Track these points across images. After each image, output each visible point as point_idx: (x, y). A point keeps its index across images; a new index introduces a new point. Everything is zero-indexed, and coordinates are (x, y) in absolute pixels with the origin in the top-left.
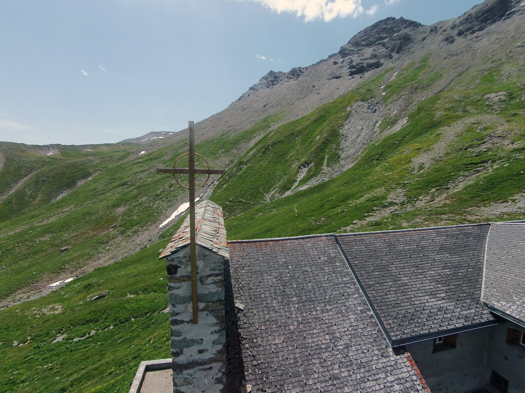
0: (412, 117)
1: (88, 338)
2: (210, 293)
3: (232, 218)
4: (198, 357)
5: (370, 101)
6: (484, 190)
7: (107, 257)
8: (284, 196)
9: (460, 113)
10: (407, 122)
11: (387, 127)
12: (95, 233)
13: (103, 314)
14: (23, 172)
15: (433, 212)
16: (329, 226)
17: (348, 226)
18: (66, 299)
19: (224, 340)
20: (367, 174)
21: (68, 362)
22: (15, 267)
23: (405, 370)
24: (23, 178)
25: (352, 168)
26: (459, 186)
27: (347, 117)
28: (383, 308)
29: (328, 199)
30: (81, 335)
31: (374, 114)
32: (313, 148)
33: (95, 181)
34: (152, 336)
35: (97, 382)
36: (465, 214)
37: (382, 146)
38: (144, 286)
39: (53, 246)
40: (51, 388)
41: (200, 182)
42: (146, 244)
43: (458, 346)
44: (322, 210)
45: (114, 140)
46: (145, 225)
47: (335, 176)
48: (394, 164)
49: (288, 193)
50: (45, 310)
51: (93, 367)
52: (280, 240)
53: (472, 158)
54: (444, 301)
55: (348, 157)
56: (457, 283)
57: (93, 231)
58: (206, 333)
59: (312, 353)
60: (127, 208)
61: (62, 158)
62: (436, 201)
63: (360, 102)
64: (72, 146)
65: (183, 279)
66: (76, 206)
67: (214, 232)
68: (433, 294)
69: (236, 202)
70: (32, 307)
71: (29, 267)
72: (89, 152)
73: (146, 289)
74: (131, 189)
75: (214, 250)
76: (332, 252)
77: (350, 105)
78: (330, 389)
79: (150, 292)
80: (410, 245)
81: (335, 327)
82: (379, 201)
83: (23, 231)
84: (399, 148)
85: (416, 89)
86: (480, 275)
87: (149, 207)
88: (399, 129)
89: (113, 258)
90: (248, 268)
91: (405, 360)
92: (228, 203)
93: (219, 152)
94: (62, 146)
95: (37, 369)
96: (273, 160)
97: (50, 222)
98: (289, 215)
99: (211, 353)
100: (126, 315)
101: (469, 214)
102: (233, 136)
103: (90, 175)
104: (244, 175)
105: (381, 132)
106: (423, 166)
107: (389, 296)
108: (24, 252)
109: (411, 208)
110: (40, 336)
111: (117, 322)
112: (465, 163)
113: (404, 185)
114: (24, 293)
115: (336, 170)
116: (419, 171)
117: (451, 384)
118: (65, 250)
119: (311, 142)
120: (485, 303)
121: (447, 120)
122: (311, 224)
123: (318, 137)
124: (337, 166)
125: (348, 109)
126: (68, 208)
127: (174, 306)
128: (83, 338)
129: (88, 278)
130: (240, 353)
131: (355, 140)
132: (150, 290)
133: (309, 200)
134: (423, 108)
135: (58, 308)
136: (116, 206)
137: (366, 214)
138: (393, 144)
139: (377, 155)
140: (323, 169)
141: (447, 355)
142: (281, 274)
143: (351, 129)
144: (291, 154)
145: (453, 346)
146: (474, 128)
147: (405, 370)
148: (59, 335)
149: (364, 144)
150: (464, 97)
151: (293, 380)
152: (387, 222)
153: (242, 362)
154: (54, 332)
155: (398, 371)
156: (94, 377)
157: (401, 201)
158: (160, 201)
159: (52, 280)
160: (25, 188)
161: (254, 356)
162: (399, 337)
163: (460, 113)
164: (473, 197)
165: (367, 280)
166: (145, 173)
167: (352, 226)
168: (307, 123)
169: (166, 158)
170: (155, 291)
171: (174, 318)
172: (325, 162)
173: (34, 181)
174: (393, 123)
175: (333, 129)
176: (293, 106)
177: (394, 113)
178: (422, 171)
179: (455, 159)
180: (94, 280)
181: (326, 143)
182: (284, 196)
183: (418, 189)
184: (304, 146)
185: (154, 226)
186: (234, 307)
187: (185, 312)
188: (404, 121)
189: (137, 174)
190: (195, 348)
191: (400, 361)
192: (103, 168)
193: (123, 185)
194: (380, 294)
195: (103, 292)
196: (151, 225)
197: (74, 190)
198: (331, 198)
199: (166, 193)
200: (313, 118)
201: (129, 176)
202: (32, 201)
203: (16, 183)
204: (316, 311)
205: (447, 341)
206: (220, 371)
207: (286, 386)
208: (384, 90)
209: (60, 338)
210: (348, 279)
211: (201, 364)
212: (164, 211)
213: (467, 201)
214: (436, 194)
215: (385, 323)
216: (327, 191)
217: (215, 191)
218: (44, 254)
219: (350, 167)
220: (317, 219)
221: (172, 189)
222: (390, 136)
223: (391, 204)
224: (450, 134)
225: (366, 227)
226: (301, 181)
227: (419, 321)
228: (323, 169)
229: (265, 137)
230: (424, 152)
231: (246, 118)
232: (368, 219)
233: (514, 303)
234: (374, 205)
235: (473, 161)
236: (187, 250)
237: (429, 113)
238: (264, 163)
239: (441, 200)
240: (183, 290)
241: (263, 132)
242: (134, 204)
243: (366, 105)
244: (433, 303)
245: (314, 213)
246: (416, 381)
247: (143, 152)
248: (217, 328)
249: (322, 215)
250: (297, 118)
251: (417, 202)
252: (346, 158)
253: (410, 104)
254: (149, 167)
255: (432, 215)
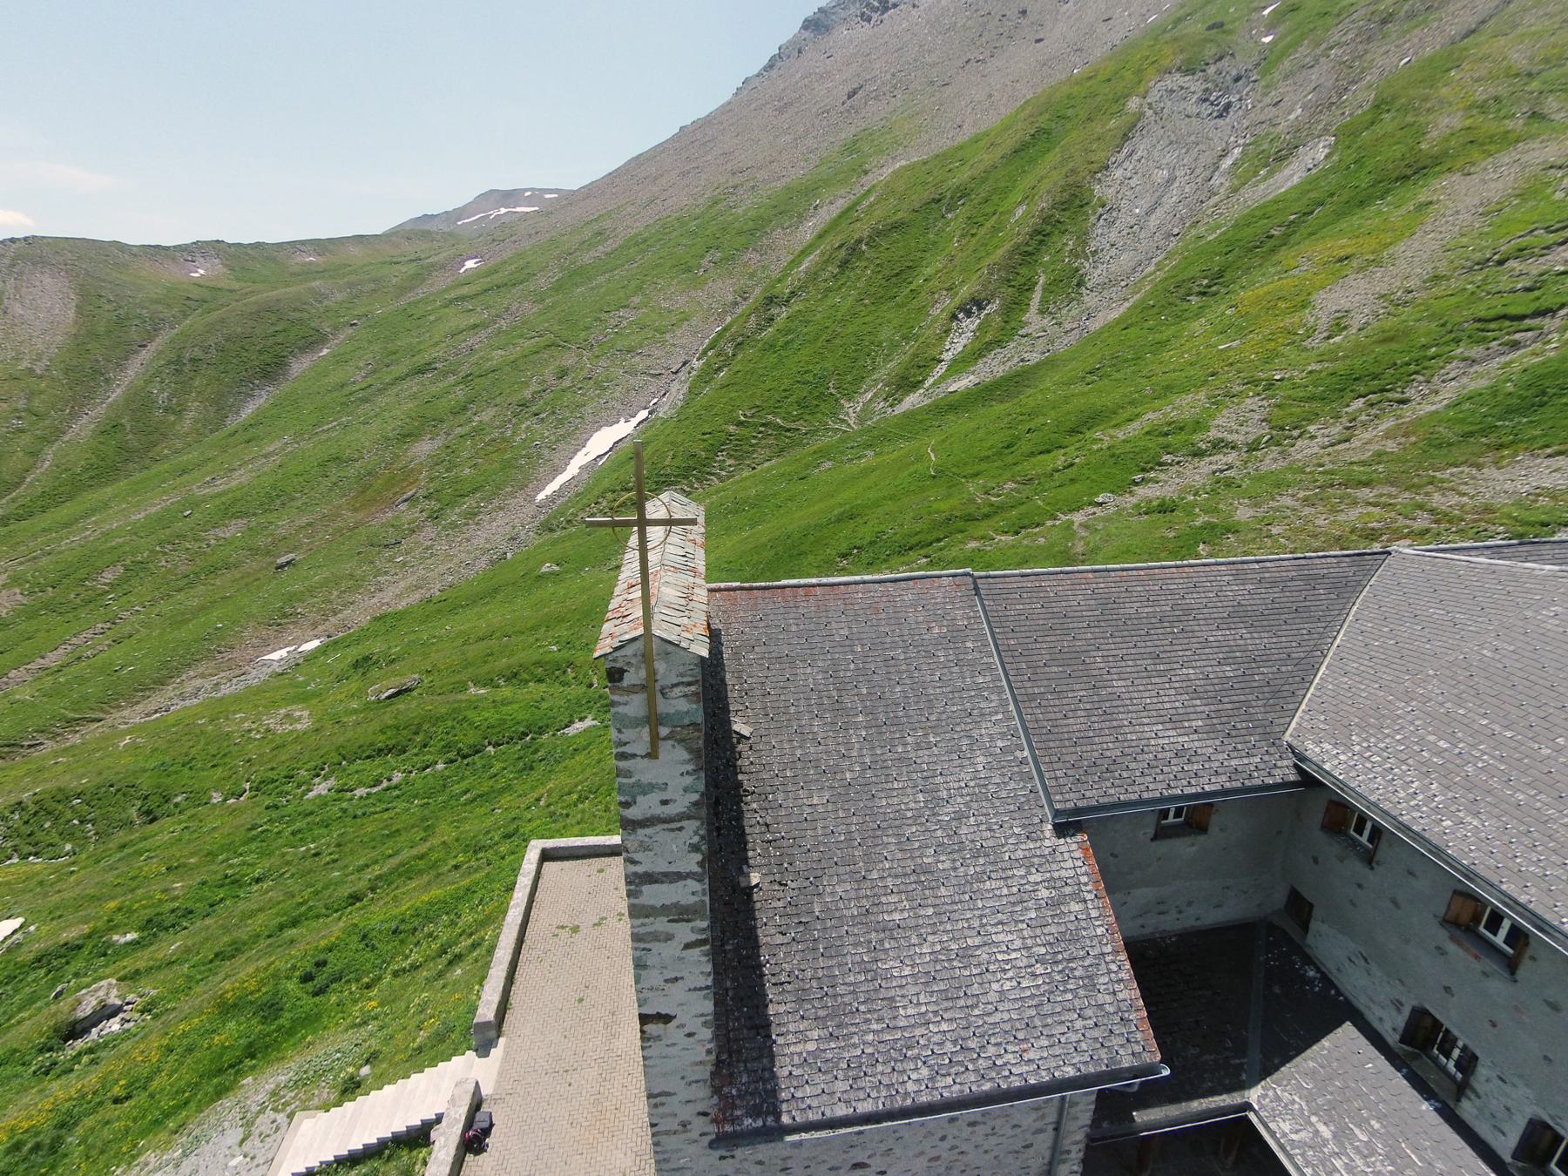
0: (1347, 135)
1: (388, 789)
2: (678, 713)
3: (745, 474)
4: (660, 811)
5: (1212, 70)
6: (1509, 412)
7: (402, 584)
8: (899, 409)
9: (1516, 124)
10: (1327, 157)
11: (1256, 173)
12: (360, 516)
13: (416, 733)
14: (134, 335)
15: (1337, 479)
16: (1023, 509)
17: (1078, 509)
18: (315, 694)
19: (702, 787)
20: (1162, 344)
21: (351, 841)
22: (165, 607)
23: (1069, 864)
24: (136, 352)
25: (1118, 321)
26: (1432, 399)
27: (1126, 137)
28: (1052, 744)
29: (1032, 425)
30: (370, 781)
31: (1220, 122)
32: (1000, 252)
33: (340, 359)
34: (541, 790)
35: (429, 884)
36: (1430, 488)
37: (1229, 244)
38: (509, 667)
39: (254, 551)
40: (327, 893)
41: (649, 362)
42: (503, 548)
43: (1214, 829)
44: (1010, 459)
45: (377, 223)
46: (495, 494)
47: (1060, 347)
48: (1254, 311)
49: (912, 400)
50: (271, 722)
51: (414, 852)
52: (840, 584)
53: (1508, 298)
54: (1195, 737)
55: (1110, 283)
56: (1243, 698)
57: (355, 510)
58: (674, 777)
59: (884, 825)
60: (440, 442)
61: (236, 286)
62: (1355, 443)
63: (1178, 75)
64: (258, 246)
65: (632, 689)
66: (297, 438)
67: (683, 602)
68: (1173, 721)
69: (755, 425)
70: (235, 713)
71: (202, 609)
72: (311, 263)
73: (515, 675)
74: (446, 383)
75: (683, 645)
76: (960, 616)
77: (1141, 89)
78: (910, 888)
79: (527, 682)
80: (1156, 603)
81: (939, 779)
82: (1182, 437)
83: (167, 510)
84: (1283, 253)
85: (1384, 22)
86: (1306, 682)
87: (505, 440)
88: (1296, 180)
89: (417, 588)
90: (763, 649)
91: (1074, 847)
92: (732, 428)
93: (704, 262)
94: (230, 245)
95: (283, 855)
96: (873, 290)
97: (234, 484)
98: (912, 469)
99: (682, 803)
100: (472, 738)
101: (1441, 489)
102: (746, 206)
103: (322, 340)
104: (782, 340)
105: (1235, 190)
106: (1344, 323)
107: (1071, 721)
108: (183, 569)
109: (1275, 460)
110: (273, 781)
111: (451, 755)
112: (1482, 314)
113: (1270, 385)
114: (203, 676)
115: (1068, 327)
116: (1328, 338)
117: (1190, 904)
118: (288, 563)
119: (995, 230)
120: (1290, 746)
121: (1477, 144)
122: (972, 501)
123: (1020, 212)
124: (1074, 312)
125: (1133, 104)
126: (278, 444)
127: (620, 731)
128: (375, 790)
129: (358, 641)
130: (739, 816)
131: (1140, 223)
132: (525, 676)
133: (973, 424)
134: (1394, 98)
135: (300, 719)
136: (407, 436)
137: (1138, 477)
138: (1262, 239)
139: (1205, 278)
140: (1028, 323)
141: (1185, 848)
142: (834, 662)
143: (1132, 183)
144: (929, 271)
145: (1202, 829)
146: (1548, 184)
147: (1069, 864)
148: (317, 780)
149: (1169, 235)
150: (1546, 60)
151: (841, 870)
152: (1194, 505)
153: (743, 834)
154: (303, 772)
155: (1054, 867)
156: (420, 872)
157: (1251, 438)
158: (535, 419)
159: (267, 645)
160: (147, 382)
161: (767, 825)
162: (1070, 805)
163: (1516, 124)
164: (1471, 434)
165: (1029, 684)
166: (483, 334)
167: (1091, 510)
168: (987, 158)
169: (543, 282)
170: (540, 681)
171: (621, 750)
172: (1037, 296)
173: (170, 362)
174: (1281, 157)
175: (1071, 180)
176: (948, 90)
177: (1292, 117)
178: (1338, 339)
179: (1453, 300)
180: (376, 647)
181: (1042, 234)
182: (899, 409)
183: (1311, 399)
184: (974, 241)
185: (521, 495)
186: (730, 731)
187: (639, 741)
188: (1318, 152)
189: (461, 337)
190: (655, 797)
191: (1063, 849)
192: (359, 317)
193: (421, 371)
194: (1053, 716)
195: (408, 680)
196: (513, 495)
197: (286, 387)
198: (1041, 420)
199: (547, 396)
200: (1009, 143)
201: (437, 344)
202: (173, 424)
203: (120, 367)
204: (905, 745)
205: (1193, 817)
206: (696, 833)
207: (825, 878)
208: (1271, 26)
209: (321, 788)
210: (988, 679)
211: (665, 821)
212: (546, 452)
213: (1450, 445)
214: (1363, 418)
215: (1047, 775)
216: (1029, 398)
217: (693, 392)
218: (236, 574)
219: (1114, 315)
220: (990, 485)
221: (567, 383)
222: (1264, 206)
223: (1218, 446)
224: (1462, 203)
225: (1130, 515)
226: (954, 360)
227: (1125, 775)
228: (1028, 323)
229: (849, 209)
230: (1361, 269)
231: (789, 138)
232: (1141, 491)
233: (1349, 748)
234: (1167, 449)
235: (1513, 310)
236: (639, 645)
237: (1409, 119)
238: (843, 300)
239: (1376, 436)
240: (634, 706)
241: (842, 191)
242: (459, 430)
243: (1195, 85)
244: (1173, 738)
245: (984, 466)
246: (1086, 884)
247: (470, 264)
248: (690, 767)
249: (1008, 475)
250: (960, 140)
251: (1299, 443)
252: (1103, 286)
253: (1354, 82)
254: (493, 312)
255: (1332, 486)
